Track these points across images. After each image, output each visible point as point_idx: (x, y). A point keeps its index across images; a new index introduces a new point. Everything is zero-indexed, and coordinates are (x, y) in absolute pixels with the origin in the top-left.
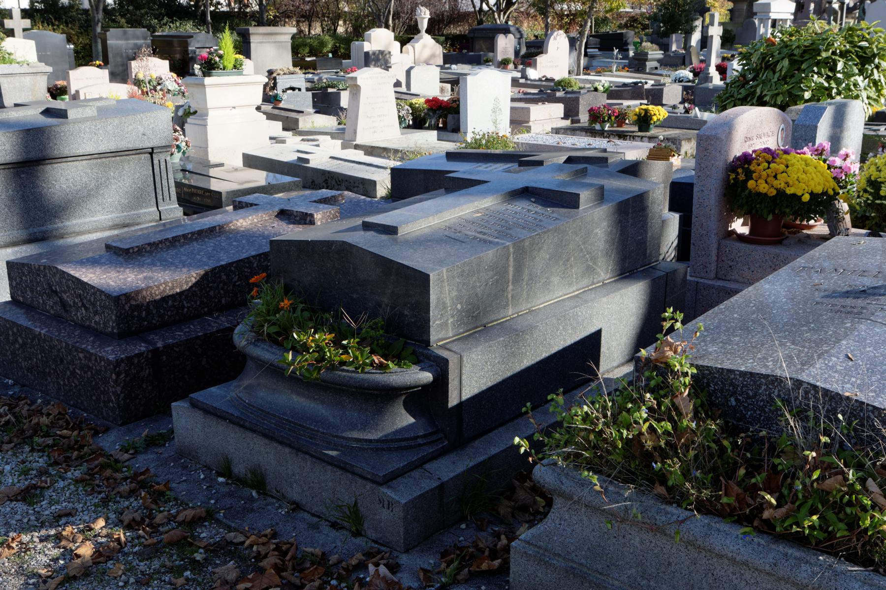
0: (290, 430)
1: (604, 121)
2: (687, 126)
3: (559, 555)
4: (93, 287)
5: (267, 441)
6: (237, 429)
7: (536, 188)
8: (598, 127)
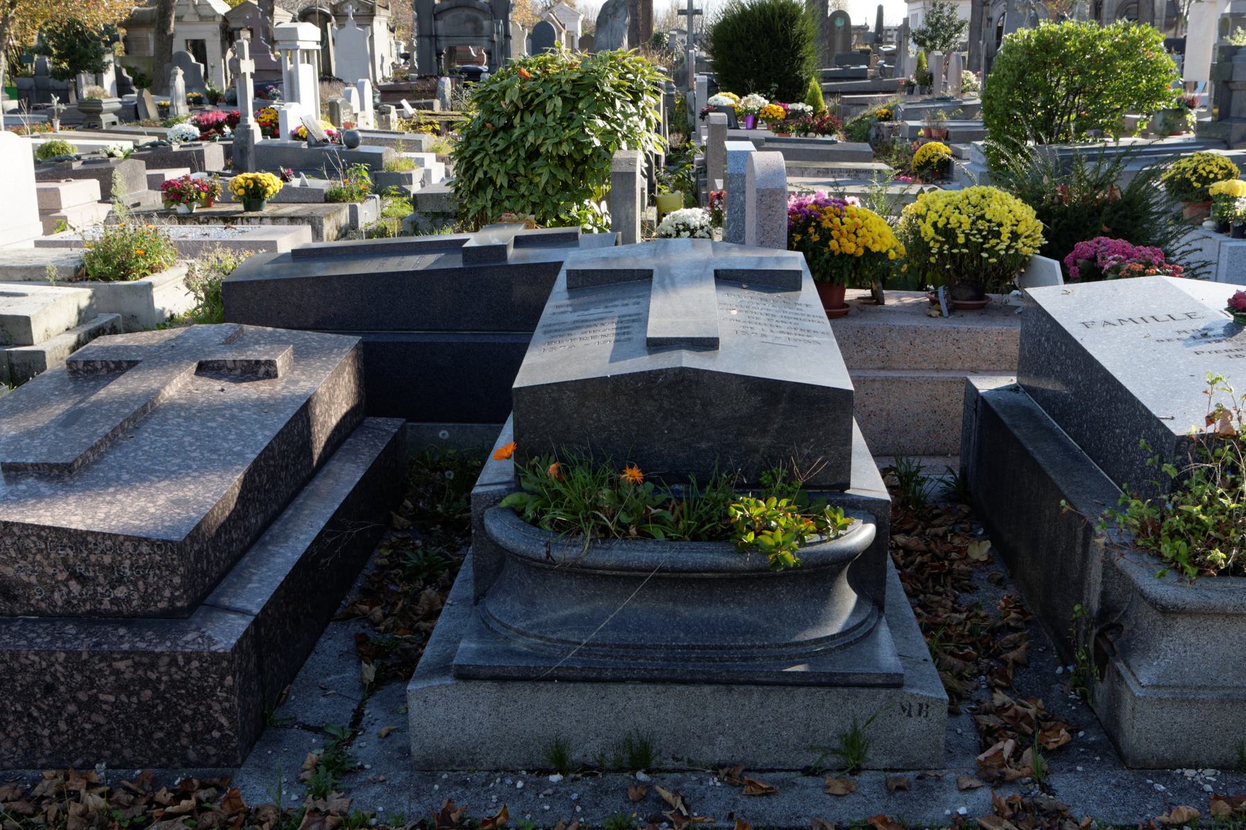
0: (698, 659)
1: (192, 200)
2: (295, 198)
3: (1205, 687)
4: (111, 536)
5: (659, 688)
6: (588, 688)
7: (731, 271)
8: (182, 209)
